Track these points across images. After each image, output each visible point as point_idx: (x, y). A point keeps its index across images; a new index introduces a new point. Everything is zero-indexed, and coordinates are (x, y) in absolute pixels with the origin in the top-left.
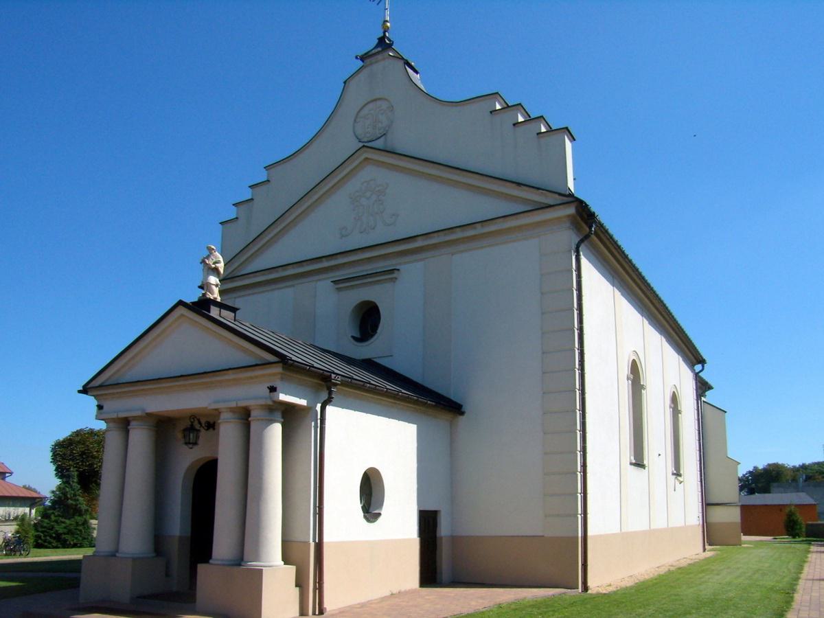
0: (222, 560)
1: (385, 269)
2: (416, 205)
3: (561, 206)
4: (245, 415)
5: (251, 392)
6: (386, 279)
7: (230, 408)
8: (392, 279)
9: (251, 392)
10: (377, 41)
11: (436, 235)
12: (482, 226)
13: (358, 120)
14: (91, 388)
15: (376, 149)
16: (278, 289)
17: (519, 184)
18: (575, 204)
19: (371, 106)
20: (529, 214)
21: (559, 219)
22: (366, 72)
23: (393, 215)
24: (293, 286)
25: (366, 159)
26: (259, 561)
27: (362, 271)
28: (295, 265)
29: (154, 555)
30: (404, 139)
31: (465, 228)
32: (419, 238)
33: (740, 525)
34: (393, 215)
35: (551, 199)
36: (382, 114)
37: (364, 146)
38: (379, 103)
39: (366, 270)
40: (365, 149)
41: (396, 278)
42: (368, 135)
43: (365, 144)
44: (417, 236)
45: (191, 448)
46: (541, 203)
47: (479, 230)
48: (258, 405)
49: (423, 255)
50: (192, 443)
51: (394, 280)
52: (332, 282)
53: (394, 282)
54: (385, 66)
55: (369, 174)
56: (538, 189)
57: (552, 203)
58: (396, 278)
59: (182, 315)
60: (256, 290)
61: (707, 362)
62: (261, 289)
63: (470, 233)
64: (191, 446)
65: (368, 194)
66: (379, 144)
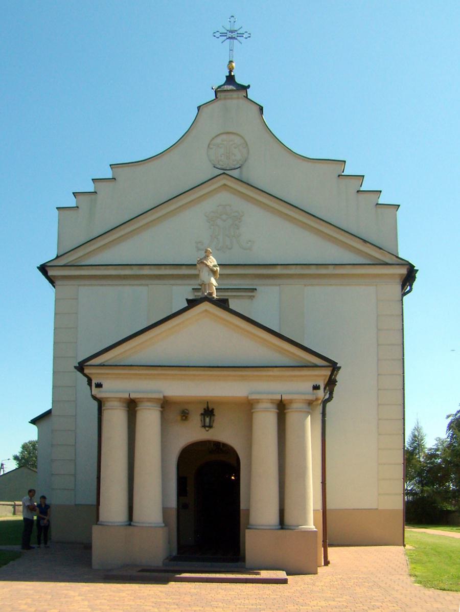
0: (269, 526)
1: (239, 287)
2: (270, 238)
3: (397, 266)
4: (282, 408)
5: (267, 389)
6: (245, 296)
7: (271, 399)
8: (251, 296)
9: (267, 389)
10: (225, 79)
11: (294, 267)
12: (334, 268)
13: (211, 146)
14: (87, 366)
15: (230, 176)
16: (130, 285)
17: (365, 241)
18: (407, 267)
19: (224, 137)
20: (373, 266)
21: (393, 275)
22: (218, 104)
23: (250, 241)
24: (147, 285)
25: (225, 185)
26: (307, 525)
27: (241, 285)
28: (152, 267)
29: (163, 525)
30: (258, 173)
31: (319, 266)
32: (279, 267)
33: (402, 511)
34: (250, 241)
35: (387, 259)
36: (235, 148)
37: (224, 173)
38: (232, 137)
39: (235, 285)
40: (225, 176)
41: (254, 296)
42: (221, 163)
43: (225, 172)
44: (278, 265)
45: (207, 431)
46: (380, 260)
47: (330, 271)
48: (268, 399)
49: (278, 281)
50: (207, 427)
51: (252, 297)
52: (193, 289)
53: (252, 299)
54: (234, 102)
55: (224, 197)
56: (381, 249)
57: (390, 262)
58: (254, 296)
59: (206, 311)
60: (124, 282)
61: (312, 386)
62: (110, 282)
63: (323, 271)
64: (207, 429)
65: (224, 217)
66: (235, 173)
